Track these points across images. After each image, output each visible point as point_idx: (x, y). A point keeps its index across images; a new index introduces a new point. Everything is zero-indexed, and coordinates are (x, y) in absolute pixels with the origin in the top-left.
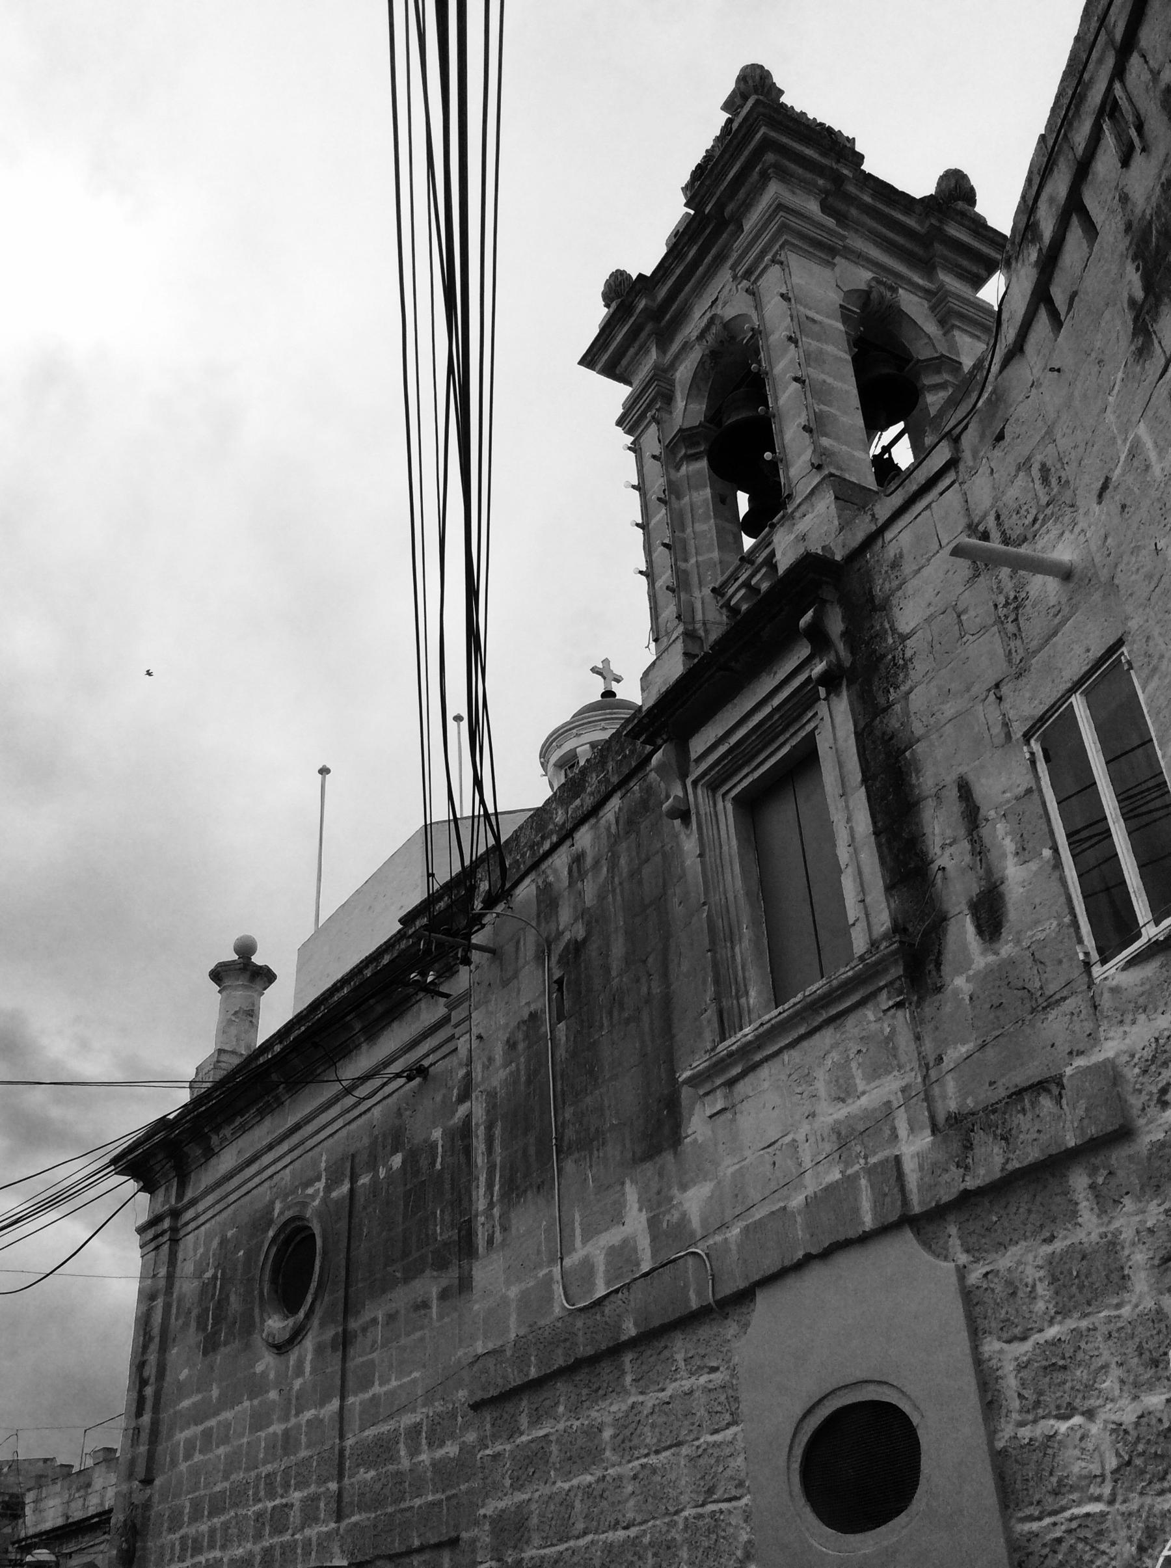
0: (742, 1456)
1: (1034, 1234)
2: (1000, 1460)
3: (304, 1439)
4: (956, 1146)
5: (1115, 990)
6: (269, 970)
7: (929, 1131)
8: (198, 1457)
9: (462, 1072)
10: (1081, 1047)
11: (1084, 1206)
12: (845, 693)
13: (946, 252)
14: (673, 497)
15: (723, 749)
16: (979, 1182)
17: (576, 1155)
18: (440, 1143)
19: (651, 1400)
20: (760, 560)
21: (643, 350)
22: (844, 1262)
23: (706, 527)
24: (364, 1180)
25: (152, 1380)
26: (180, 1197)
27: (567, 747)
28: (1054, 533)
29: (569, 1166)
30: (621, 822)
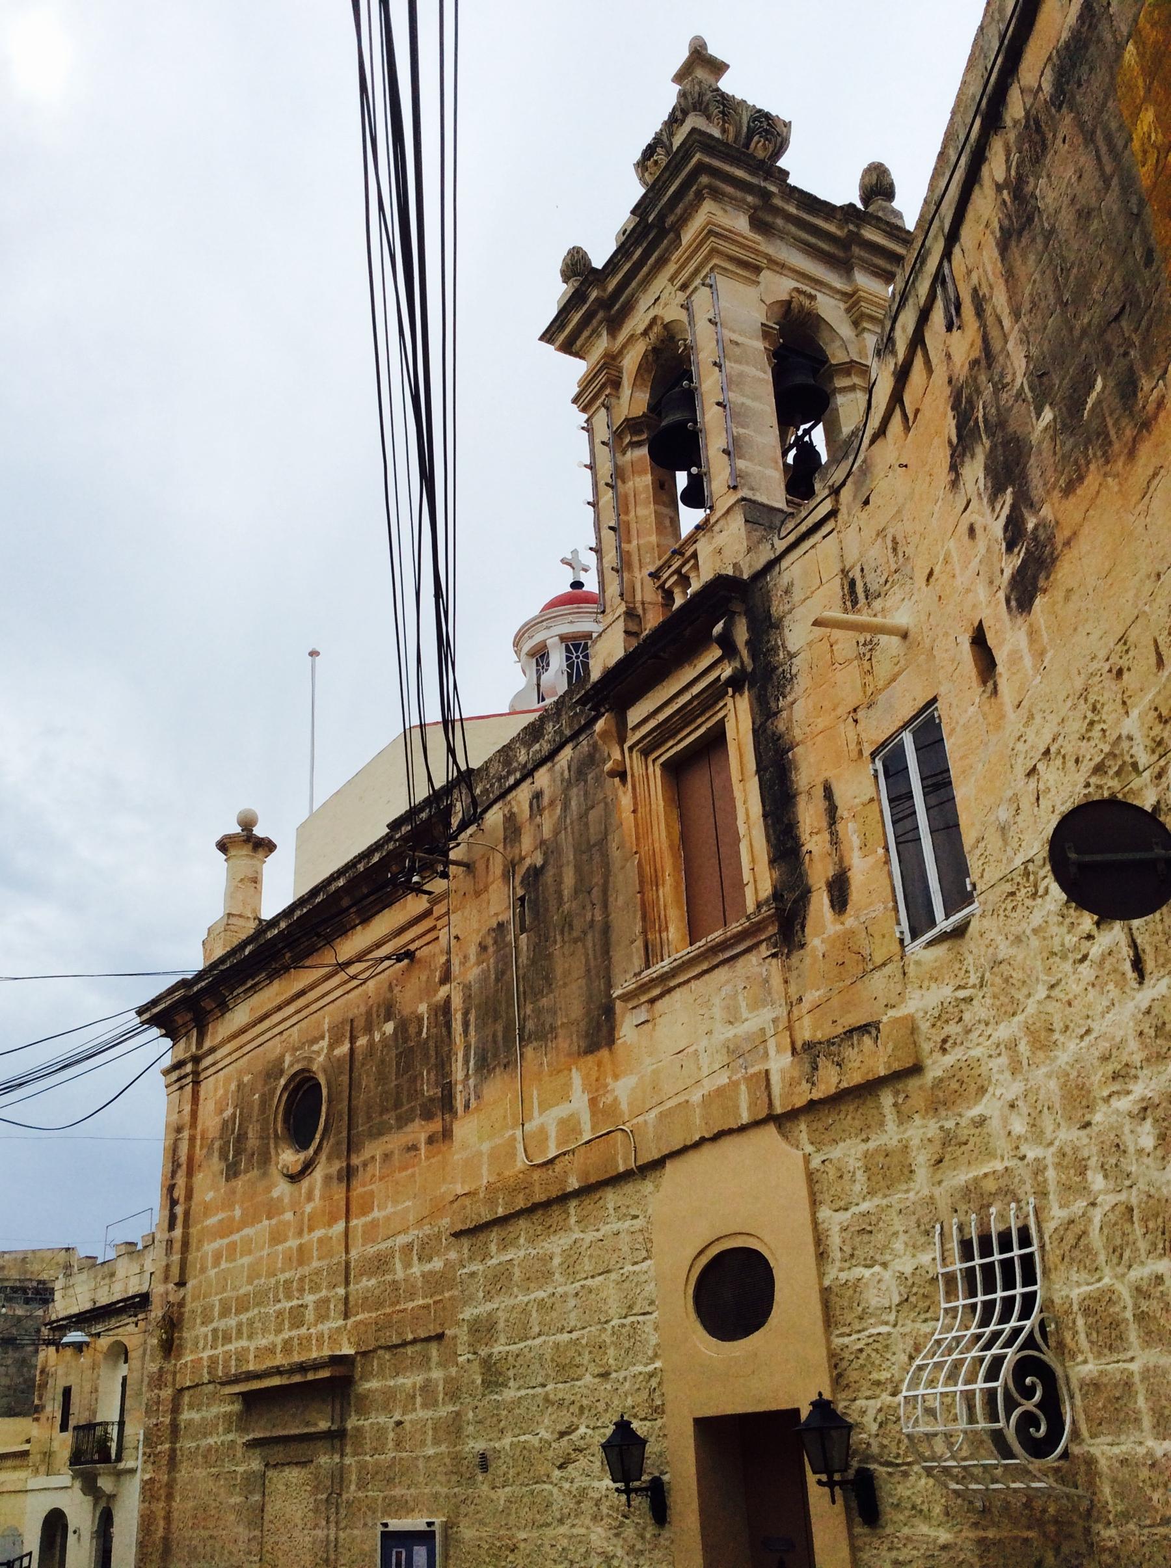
0: (653, 1284)
1: (856, 1136)
2: (825, 1292)
3: (315, 1254)
4: (807, 1067)
5: (918, 963)
6: (270, 841)
7: (789, 1053)
8: (224, 1265)
9: (443, 959)
10: (892, 1002)
11: (889, 1117)
12: (746, 693)
13: (862, 253)
14: (619, 482)
15: (652, 724)
16: (821, 1095)
17: (535, 1044)
18: (426, 1016)
19: (590, 1236)
20: (688, 554)
21: (596, 333)
22: (727, 1143)
23: (645, 512)
24: (362, 1041)
25: (182, 1200)
26: (200, 1044)
27: (538, 638)
28: (899, 596)
29: (529, 1051)
30: (572, 769)
